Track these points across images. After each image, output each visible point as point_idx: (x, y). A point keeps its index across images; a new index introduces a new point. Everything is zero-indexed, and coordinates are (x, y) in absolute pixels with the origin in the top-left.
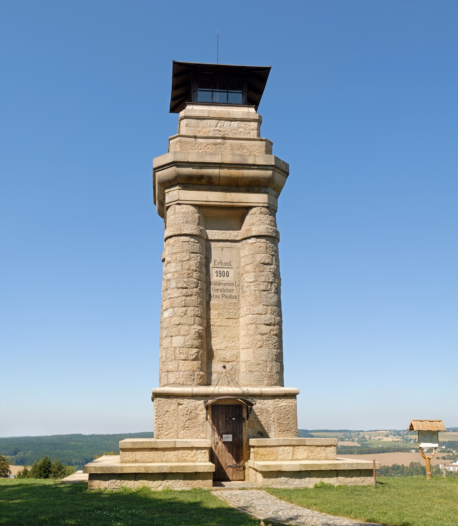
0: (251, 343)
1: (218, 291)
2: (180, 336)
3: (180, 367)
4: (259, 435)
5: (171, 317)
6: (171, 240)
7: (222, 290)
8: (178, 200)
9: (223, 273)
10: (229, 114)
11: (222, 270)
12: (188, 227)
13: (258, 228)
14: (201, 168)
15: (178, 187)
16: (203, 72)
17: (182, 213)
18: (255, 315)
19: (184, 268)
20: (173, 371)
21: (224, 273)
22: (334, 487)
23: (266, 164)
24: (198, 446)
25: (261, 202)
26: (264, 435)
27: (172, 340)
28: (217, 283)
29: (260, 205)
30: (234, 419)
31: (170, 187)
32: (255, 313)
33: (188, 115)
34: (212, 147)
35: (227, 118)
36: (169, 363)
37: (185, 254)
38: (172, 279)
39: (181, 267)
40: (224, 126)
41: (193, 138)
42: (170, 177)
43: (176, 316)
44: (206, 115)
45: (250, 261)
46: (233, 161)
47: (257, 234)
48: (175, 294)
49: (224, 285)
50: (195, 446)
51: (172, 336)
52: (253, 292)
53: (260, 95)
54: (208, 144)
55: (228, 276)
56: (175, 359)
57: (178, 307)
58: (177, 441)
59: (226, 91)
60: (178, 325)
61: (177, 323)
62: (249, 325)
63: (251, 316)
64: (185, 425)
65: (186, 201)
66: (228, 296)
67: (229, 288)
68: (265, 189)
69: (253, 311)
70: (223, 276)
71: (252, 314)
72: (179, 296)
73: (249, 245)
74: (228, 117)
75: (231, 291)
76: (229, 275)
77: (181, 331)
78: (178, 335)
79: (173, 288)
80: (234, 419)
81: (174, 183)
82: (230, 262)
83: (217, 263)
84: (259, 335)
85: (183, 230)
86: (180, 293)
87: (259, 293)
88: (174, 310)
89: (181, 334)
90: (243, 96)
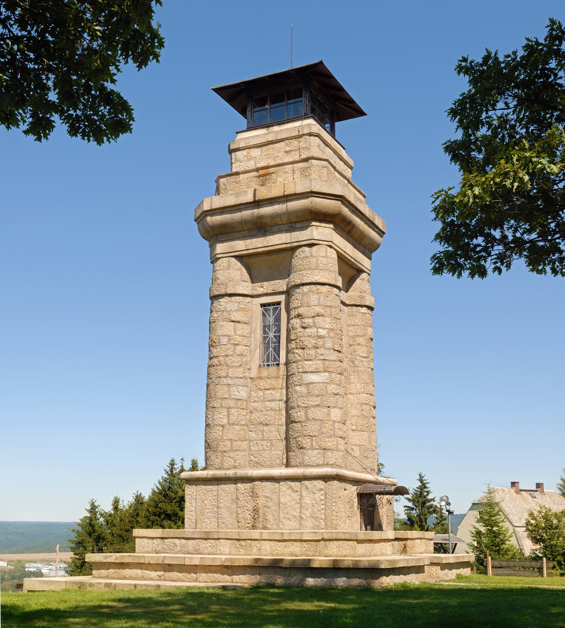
5: (326, 383)
6: (322, 288)
8: (332, 242)
14: (353, 212)
15: (332, 226)
16: (318, 87)
20: (332, 450)
25: (279, 243)
27: (329, 411)
31: (321, 221)
32: (368, 392)
36: (327, 439)
38: (326, 337)
42: (330, 211)
43: (334, 384)
48: (332, 357)
51: (329, 407)
56: (334, 436)
57: (335, 373)
60: (336, 395)
61: (336, 392)
62: (364, 405)
63: (366, 395)
65: (337, 246)
73: (361, 314)
78: (335, 407)
79: (329, 349)
81: (330, 220)
88: (330, 377)
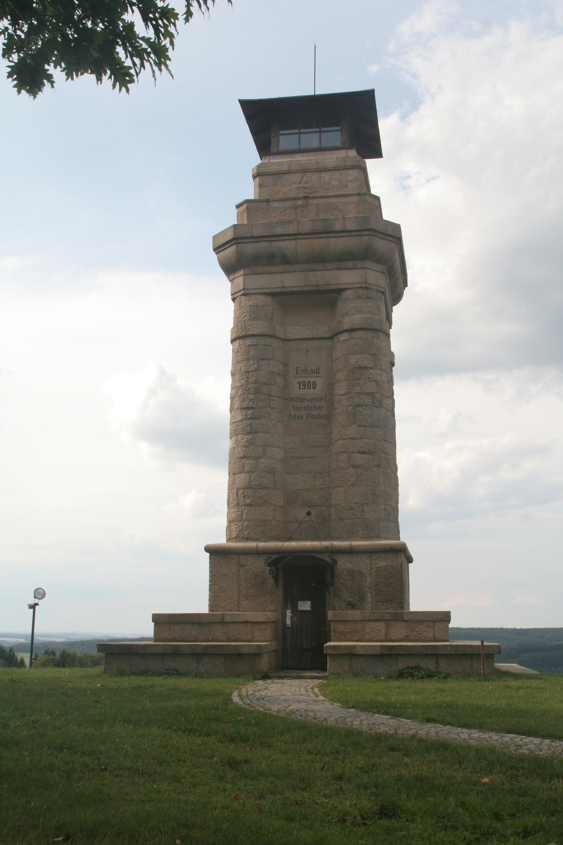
0: (342, 479)
1: (302, 409)
2: (245, 473)
3: (244, 516)
4: (349, 606)
7: (307, 408)
10: (318, 163)
11: (307, 380)
12: (255, 326)
13: (351, 319)
17: (248, 306)
18: (347, 440)
19: (250, 381)
22: (268, 656)
23: (359, 229)
24: (254, 620)
26: (355, 607)
28: (300, 399)
29: (355, 287)
30: (313, 584)
32: (346, 437)
33: (261, 172)
34: (290, 212)
35: (315, 169)
37: (251, 362)
39: (246, 380)
40: (311, 181)
41: (265, 202)
44: (285, 168)
45: (341, 365)
47: (350, 327)
49: (309, 400)
50: (250, 620)
52: (345, 408)
54: (285, 209)
55: (315, 388)
58: (225, 614)
63: (342, 442)
64: (248, 593)
66: (314, 416)
67: (317, 404)
69: (345, 434)
70: (308, 388)
71: (343, 439)
72: (243, 419)
74: (316, 168)
75: (318, 408)
76: (317, 387)
77: (246, 467)
80: (313, 584)
82: (319, 369)
83: (300, 372)
84: (352, 467)
85: (249, 329)
87: (352, 409)
90: (341, 135)
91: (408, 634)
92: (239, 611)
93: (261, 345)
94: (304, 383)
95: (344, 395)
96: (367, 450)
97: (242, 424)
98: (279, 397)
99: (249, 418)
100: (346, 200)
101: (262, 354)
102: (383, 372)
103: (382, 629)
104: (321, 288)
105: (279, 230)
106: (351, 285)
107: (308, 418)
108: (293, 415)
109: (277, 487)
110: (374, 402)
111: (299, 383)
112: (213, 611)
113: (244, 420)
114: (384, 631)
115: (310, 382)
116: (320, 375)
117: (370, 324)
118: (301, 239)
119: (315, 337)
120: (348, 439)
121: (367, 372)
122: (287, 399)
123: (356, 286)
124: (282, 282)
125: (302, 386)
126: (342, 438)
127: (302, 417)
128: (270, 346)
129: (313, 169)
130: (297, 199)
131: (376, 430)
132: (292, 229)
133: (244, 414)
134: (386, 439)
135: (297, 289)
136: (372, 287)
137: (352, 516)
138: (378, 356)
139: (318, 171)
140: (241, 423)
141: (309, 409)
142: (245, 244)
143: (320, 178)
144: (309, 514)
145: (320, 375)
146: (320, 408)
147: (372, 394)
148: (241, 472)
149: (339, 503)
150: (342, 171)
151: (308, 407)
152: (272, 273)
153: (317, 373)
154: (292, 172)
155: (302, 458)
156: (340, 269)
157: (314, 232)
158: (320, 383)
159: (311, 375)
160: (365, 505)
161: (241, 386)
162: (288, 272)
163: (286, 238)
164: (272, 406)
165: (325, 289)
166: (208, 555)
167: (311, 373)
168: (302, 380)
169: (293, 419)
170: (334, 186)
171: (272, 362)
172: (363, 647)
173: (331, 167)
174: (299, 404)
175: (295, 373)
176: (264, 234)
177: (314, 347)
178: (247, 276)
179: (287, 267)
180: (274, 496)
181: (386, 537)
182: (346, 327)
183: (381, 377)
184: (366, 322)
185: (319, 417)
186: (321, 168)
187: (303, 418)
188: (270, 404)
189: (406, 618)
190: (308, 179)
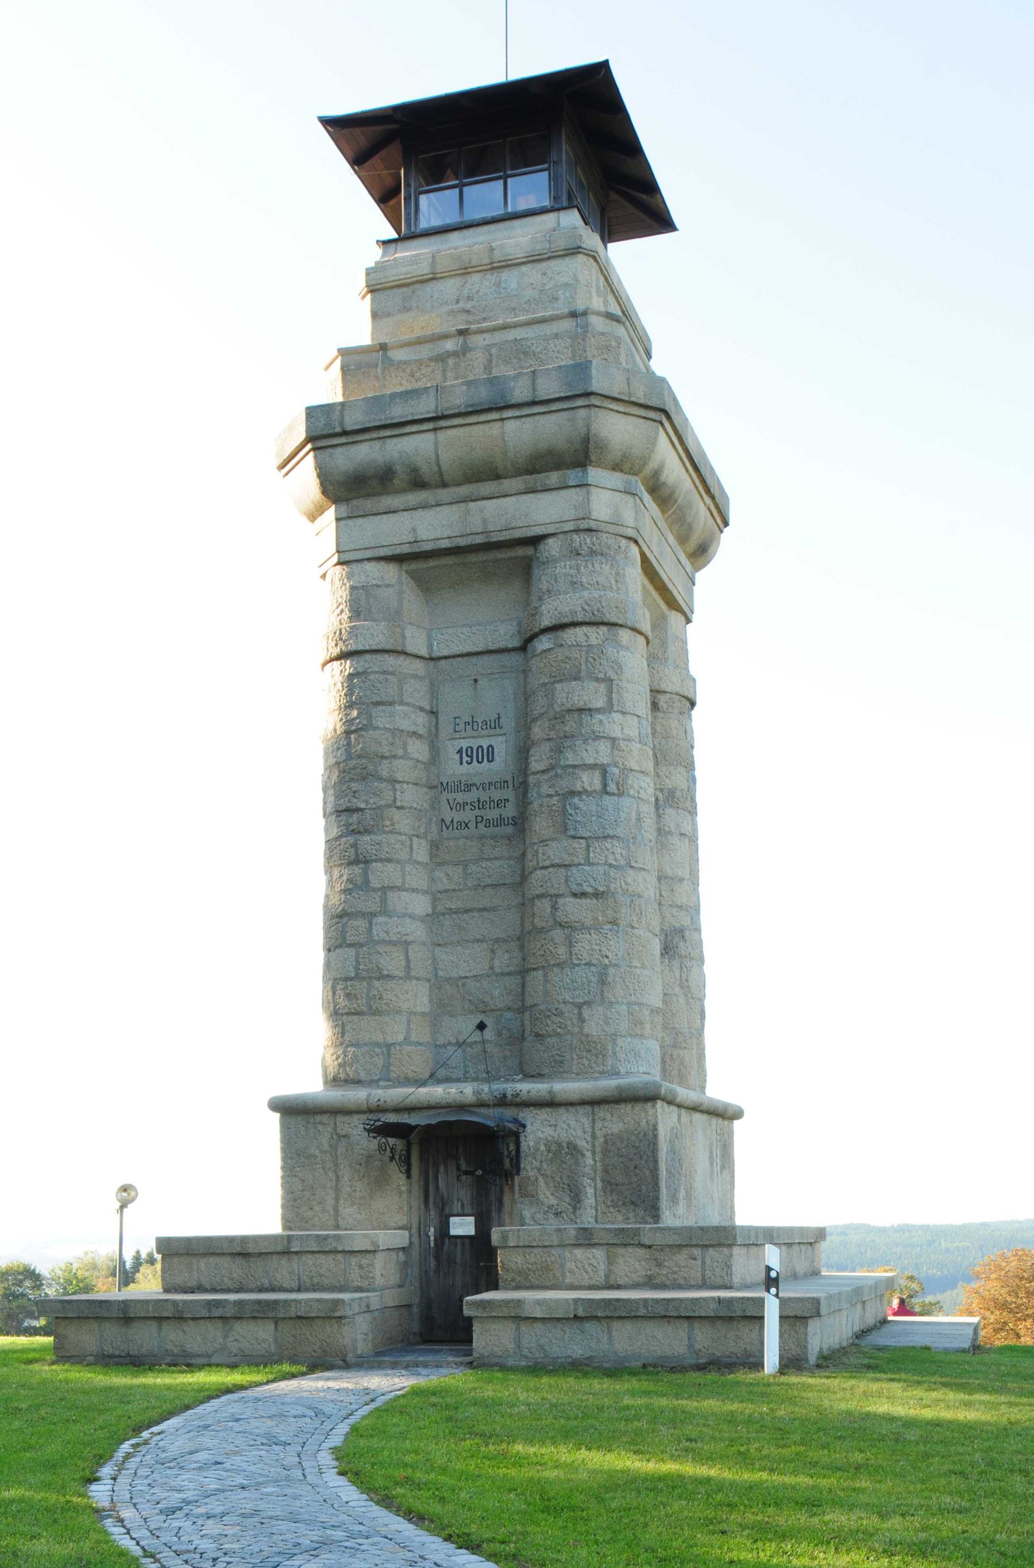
1: (466, 807)
2: (347, 947)
7: (476, 805)
9: (483, 756)
11: (474, 743)
18: (550, 870)
21: (480, 754)
29: (566, 530)
40: (480, 294)
46: (471, 403)
53: (377, 198)
59: (457, 182)
67: (496, 795)
68: (580, 474)
72: (340, 833)
75: (499, 804)
76: (496, 758)
82: (499, 718)
83: (462, 726)
86: (344, 825)
89: (348, 942)
91: (652, 1273)
92: (337, 1227)
93: (372, 672)
94: (469, 750)
95: (543, 772)
96: (589, 890)
97: (340, 845)
98: (416, 784)
99: (353, 830)
100: (548, 329)
101: (376, 691)
102: (628, 717)
103: (598, 1263)
104: (495, 538)
105: (398, 412)
106: (558, 525)
107: (479, 824)
108: (448, 820)
109: (413, 974)
110: (605, 785)
111: (460, 752)
112: (291, 1229)
113: (341, 836)
114: (602, 1267)
115: (481, 747)
116: (502, 731)
117: (596, 613)
118: (446, 428)
119: (490, 648)
120: (553, 866)
121: (589, 718)
122: (435, 787)
123: (569, 526)
124: (414, 530)
125: (465, 759)
126: (540, 865)
127: (466, 825)
128: (392, 674)
129: (482, 266)
130: (445, 337)
131: (609, 846)
132: (425, 407)
133: (342, 823)
134: (633, 864)
135: (445, 544)
136: (602, 526)
137: (559, 1030)
138: (615, 682)
139: (493, 268)
140: (338, 843)
141: (481, 807)
142: (330, 450)
143: (498, 284)
144: (481, 1026)
145: (502, 731)
146: (503, 804)
147: (604, 770)
148: (340, 946)
149: (535, 1002)
150: (544, 265)
151: (479, 801)
152: (394, 512)
153: (495, 728)
154: (438, 276)
155: (467, 911)
156: (533, 491)
157: (470, 409)
158: (502, 747)
159: (484, 733)
160: (585, 1007)
161: (336, 763)
162: (424, 506)
163: (414, 428)
164: (399, 804)
165: (502, 539)
166: (277, 1116)
167: (484, 727)
168: (465, 744)
169: (448, 828)
170: (528, 301)
171: (398, 707)
172: (539, 1303)
173: (519, 256)
174: (461, 797)
175: (452, 730)
176: (367, 425)
177: (489, 672)
178: (343, 522)
179: (422, 496)
180: (407, 993)
181: (633, 1070)
182: (546, 622)
183: (622, 729)
184: (587, 608)
185: (500, 822)
186: (499, 262)
187: (469, 825)
188: (395, 801)
189: (646, 1241)
190: (474, 291)
